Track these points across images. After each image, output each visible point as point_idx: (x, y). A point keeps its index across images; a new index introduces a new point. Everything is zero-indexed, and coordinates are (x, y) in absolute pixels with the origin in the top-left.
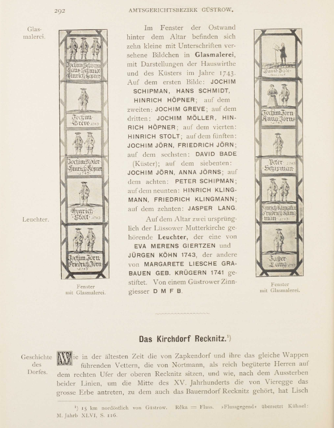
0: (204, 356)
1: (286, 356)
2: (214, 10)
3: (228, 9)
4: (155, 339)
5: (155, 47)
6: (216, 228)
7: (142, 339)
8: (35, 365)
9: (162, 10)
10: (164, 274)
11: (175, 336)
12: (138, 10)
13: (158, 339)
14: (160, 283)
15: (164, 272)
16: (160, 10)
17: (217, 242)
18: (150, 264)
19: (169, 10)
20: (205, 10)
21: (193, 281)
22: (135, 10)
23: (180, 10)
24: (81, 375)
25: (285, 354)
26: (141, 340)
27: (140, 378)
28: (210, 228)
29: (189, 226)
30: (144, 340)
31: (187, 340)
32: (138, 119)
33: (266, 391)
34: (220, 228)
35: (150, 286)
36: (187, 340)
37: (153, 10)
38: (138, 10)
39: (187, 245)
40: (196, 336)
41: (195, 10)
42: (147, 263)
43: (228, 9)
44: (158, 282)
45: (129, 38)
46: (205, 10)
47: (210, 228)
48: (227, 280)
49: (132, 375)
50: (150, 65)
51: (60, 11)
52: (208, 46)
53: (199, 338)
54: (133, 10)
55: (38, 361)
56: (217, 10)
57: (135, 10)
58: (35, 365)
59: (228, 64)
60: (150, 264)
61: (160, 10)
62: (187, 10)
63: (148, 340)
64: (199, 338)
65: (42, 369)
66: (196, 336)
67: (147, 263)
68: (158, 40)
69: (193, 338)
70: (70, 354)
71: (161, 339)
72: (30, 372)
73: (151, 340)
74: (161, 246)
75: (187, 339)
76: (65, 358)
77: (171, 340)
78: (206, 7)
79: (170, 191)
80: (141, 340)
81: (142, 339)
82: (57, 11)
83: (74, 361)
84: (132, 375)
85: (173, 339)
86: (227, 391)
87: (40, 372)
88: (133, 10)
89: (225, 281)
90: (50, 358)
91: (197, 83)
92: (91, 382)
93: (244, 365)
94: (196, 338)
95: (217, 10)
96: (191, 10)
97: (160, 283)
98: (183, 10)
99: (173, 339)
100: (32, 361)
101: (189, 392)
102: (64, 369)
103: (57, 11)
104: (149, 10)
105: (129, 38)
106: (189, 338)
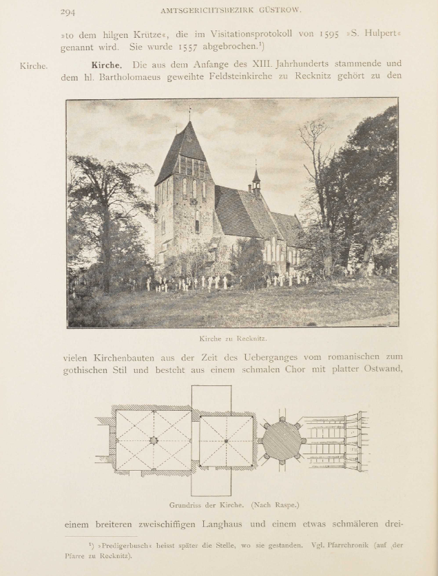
0: (132, 78)
2: (276, 10)
3: (296, 10)
5: (255, 77)
6: (261, 77)
9: (206, 10)
12: (174, 11)
19: (215, 10)
20: (263, 10)
22: (170, 11)
23: (229, 10)
28: (252, 77)
33: (355, 76)
38: (174, 11)
41: (250, 10)
43: (296, 10)
45: (399, 76)
46: (263, 10)
47: (252, 77)
50: (110, 78)
51: (68, 12)
52: (113, 78)
54: (166, 11)
56: (280, 10)
57: (170, 11)
59: (117, 78)
79: (199, 77)
82: (65, 78)
86: (301, 76)
95: (280, 10)
96: (245, 11)
103: (65, 78)
104: (189, 10)
105: (399, 76)
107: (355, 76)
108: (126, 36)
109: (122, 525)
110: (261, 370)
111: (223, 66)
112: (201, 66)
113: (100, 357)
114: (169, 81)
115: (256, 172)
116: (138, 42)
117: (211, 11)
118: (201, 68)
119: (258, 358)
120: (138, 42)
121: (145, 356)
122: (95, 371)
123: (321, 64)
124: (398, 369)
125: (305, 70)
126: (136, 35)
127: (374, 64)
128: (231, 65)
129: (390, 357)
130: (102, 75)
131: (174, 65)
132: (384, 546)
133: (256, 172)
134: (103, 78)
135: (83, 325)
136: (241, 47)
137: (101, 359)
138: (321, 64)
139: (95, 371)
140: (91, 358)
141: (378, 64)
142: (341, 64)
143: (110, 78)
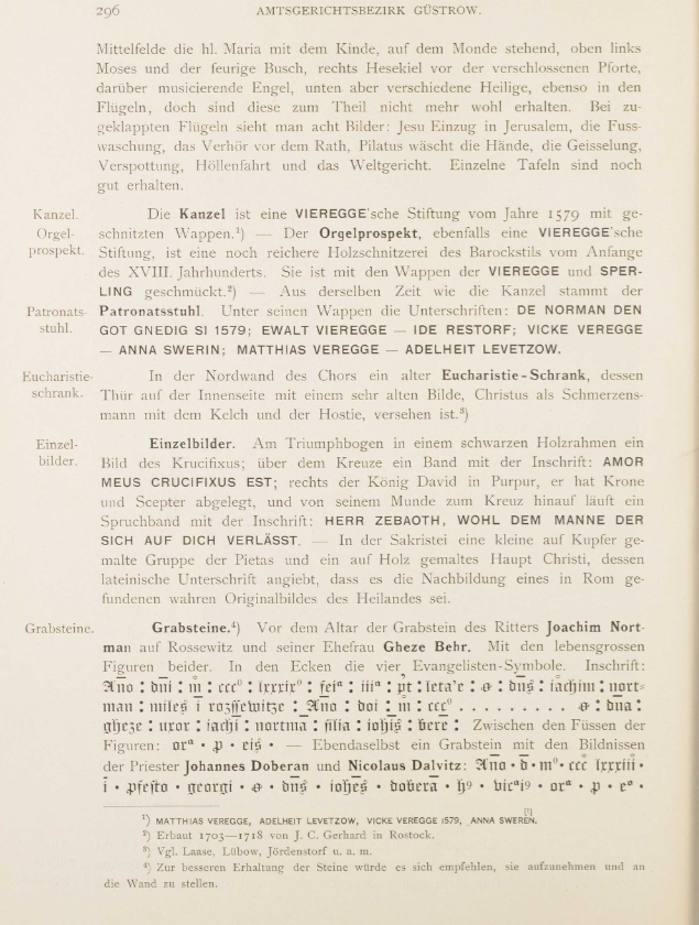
0: (469, 50)
1: (324, 313)
2: (440, 10)
3: (472, 10)
6: (411, 167)
10: (392, 522)
15: (392, 519)
16: (324, 11)
17: (564, 264)
18: (566, 519)
19: (343, 11)
25: (180, 231)
27: (325, 404)
29: (397, 498)
32: (514, 628)
34: (133, 147)
37: (309, 10)
39: (109, 540)
42: (560, 517)
43: (472, 10)
44: (109, 164)
49: (574, 49)
54: (265, 11)
56: (446, 11)
60: (566, 519)
61: (324, 11)
62: (382, 10)
67: (560, 517)
68: (418, 750)
74: (318, 213)
78: (423, 5)
84: (574, 49)
88: (265, 11)
91: (300, 600)
92: (602, 210)
98: (375, 10)
101: (428, 464)
109: (416, 254)
111: (247, 72)
112: (264, 446)
113: (346, 48)
114: (628, 584)
116: (503, 637)
118: (265, 449)
120: (503, 637)
121: (434, 308)
123: (624, 69)
125: (494, 386)
126: (498, 626)
127: (351, 747)
128: (362, 629)
131: (296, 628)
132: (620, 867)
137: (347, 51)
138: (624, 69)
140: (404, 213)
141: (160, 50)
142: (570, 292)
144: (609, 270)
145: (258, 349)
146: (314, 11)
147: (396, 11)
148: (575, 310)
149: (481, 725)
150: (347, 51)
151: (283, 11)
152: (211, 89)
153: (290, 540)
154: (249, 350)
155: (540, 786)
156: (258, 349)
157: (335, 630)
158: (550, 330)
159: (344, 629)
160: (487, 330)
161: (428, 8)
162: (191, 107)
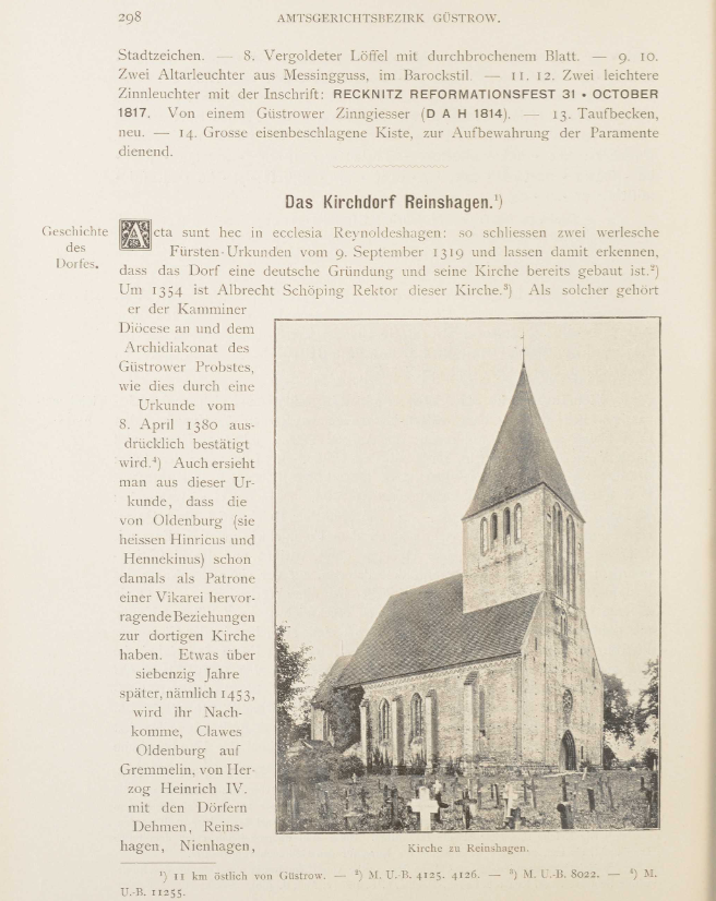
3: (491, 18)
4: (318, 202)
7: (292, 202)
8: (72, 248)
11: (362, 197)
13: (327, 202)
14: (183, 114)
16: (343, 18)
19: (363, 18)
20: (440, 18)
21: (266, 112)
22: (292, 18)
24: (258, 292)
26: (290, 204)
30: (296, 202)
31: (387, 204)
35: (252, 124)
36: (387, 204)
37: (330, 18)
40: (407, 196)
43: (491, 18)
46: (440, 18)
48: (132, 91)
51: (130, 17)
53: (414, 202)
54: (286, 18)
55: (78, 240)
56: (466, 18)
57: (292, 18)
58: (72, 248)
61: (343, 18)
63: (305, 204)
64: (414, 202)
65: (87, 256)
66: (407, 196)
69: (400, 201)
70: (145, 226)
71: (332, 202)
72: (195, 270)
73: (310, 203)
75: (389, 202)
76: (134, 234)
77: (354, 204)
80: (290, 204)
81: (292, 202)
83: (154, 241)
85: (357, 202)
87: (82, 264)
88: (286, 18)
89: (344, 113)
90: (104, 233)
92: (221, 307)
93: (531, 272)
94: (407, 201)
97: (183, 114)
99: (357, 202)
100: (66, 240)
102: (135, 258)
106: (391, 200)
107: (644, 291)
108: (532, 57)
110: (144, 580)
115: (523, 375)
117: (357, 20)
119: (157, 675)
122: (182, 57)
124: (165, 153)
129: (125, 637)
130: (409, 72)
133: (523, 375)
134: (409, 77)
135: (300, 827)
136: (626, 77)
137: (223, 638)
139: (182, 57)
143: (606, 135)
144: (521, 93)
145: (479, 94)
146: (334, 19)
147: (415, 19)
148: (457, 95)
149: (126, 74)
150: (466, 292)
151: (304, 18)
152: (651, 77)
153: (548, 94)
154: (470, 95)
155: (584, 95)
156: (479, 94)
157: (170, 77)
158: (361, 94)
159: (178, 76)
160: (442, 94)
161: (447, 16)
162: (213, 789)
